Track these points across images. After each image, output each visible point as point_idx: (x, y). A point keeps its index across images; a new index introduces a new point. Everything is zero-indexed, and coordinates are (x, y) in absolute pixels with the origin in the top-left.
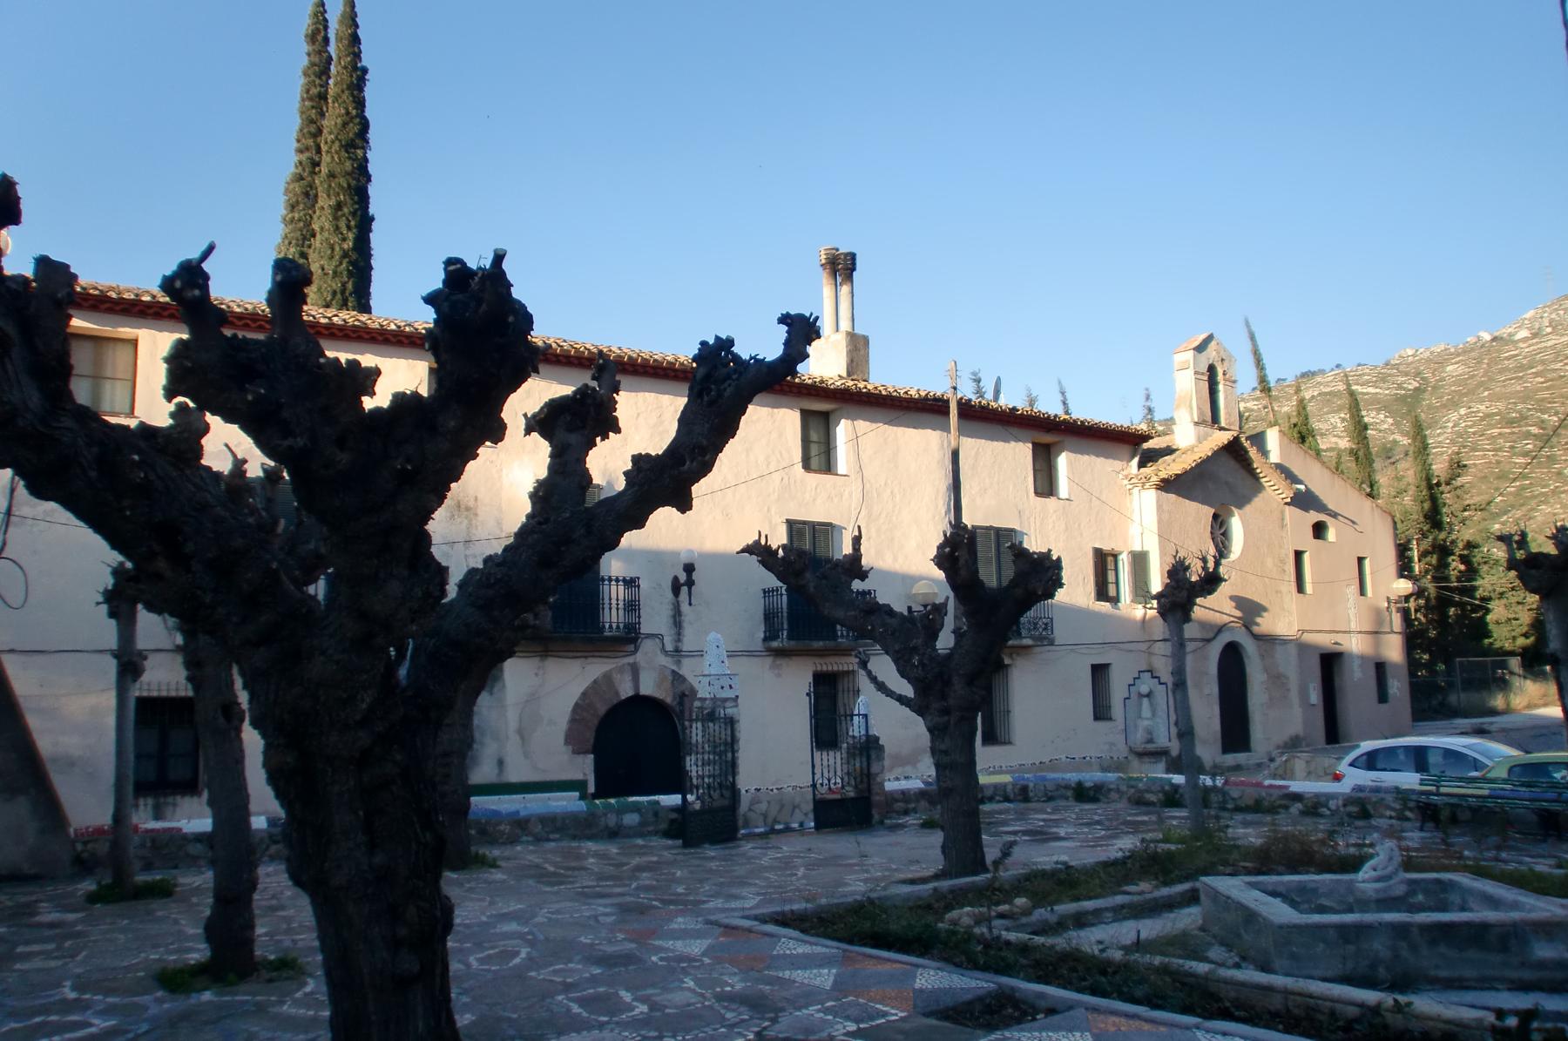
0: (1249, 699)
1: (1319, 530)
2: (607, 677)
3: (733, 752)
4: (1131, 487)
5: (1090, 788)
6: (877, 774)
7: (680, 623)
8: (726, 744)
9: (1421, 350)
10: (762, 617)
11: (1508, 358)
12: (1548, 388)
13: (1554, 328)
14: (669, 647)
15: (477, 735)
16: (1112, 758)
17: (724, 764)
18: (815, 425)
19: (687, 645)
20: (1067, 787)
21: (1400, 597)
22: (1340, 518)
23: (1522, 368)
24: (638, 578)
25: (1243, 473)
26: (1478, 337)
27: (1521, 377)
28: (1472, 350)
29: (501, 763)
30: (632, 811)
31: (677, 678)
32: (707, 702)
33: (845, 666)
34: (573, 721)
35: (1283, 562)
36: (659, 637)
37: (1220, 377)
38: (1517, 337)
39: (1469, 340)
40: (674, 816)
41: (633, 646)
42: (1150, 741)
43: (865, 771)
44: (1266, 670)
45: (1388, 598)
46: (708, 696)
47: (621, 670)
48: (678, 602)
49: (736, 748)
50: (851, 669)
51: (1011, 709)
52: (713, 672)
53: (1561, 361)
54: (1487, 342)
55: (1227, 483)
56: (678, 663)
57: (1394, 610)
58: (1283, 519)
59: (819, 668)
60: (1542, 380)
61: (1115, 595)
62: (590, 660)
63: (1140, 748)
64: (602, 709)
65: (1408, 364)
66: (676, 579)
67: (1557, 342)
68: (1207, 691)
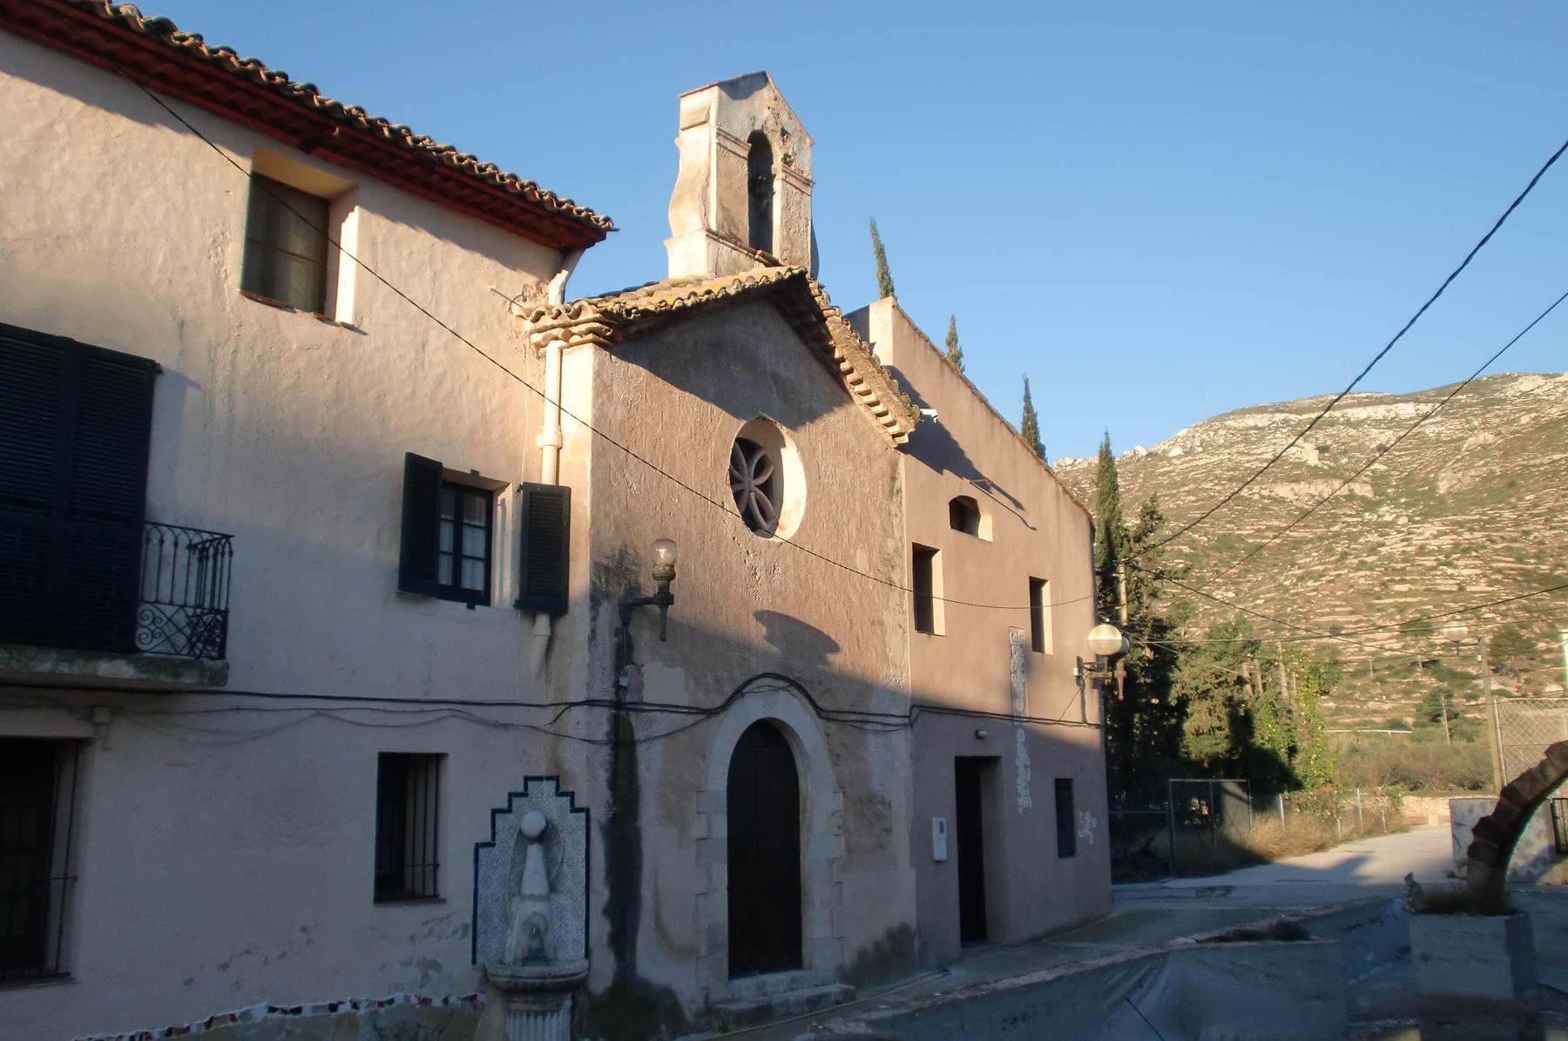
1: (963, 515)
4: (537, 338)
9: (1079, 460)
11: (1162, 474)
12: (1198, 508)
13: (1204, 448)
16: (425, 1001)
21: (1098, 657)
22: (993, 490)
23: (1175, 485)
26: (1135, 451)
27: (1175, 495)
28: (1128, 463)
37: (777, 165)
38: (1172, 454)
39: (1125, 453)
44: (842, 787)
45: (1079, 659)
51: (440, 860)
53: (1211, 481)
54: (1142, 457)
55: (776, 378)
57: (1088, 682)
58: (893, 479)
60: (1194, 499)
61: (479, 586)
63: (503, 976)
65: (1067, 473)
67: (1208, 461)
68: (697, 830)
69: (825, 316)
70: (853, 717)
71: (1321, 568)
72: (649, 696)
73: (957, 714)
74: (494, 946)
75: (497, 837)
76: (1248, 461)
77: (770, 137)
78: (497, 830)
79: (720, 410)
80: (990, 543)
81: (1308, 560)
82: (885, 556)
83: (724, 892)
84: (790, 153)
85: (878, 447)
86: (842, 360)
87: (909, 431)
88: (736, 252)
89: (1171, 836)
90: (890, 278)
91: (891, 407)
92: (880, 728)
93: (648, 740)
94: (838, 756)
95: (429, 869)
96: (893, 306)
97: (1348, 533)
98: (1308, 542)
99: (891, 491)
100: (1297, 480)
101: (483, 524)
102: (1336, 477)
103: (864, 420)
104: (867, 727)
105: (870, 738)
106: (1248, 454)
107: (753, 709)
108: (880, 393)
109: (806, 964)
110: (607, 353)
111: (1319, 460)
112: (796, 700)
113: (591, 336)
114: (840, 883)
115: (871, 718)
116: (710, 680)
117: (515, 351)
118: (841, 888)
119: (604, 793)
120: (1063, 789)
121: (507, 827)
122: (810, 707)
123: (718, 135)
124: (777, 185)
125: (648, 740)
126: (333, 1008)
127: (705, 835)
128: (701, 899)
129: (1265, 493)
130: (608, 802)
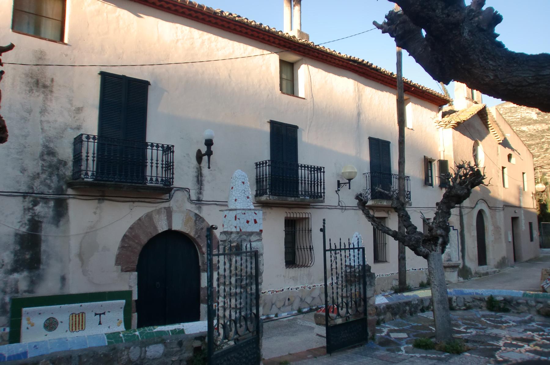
0: (486, 238)
2: (149, 216)
3: (257, 284)
5: (500, 302)
6: (369, 298)
7: (201, 181)
8: (251, 276)
10: (255, 181)
14: (194, 197)
15: (43, 257)
17: (249, 296)
18: (287, 69)
19: (206, 197)
20: (481, 300)
24: (173, 146)
25: (484, 126)
29: (63, 279)
30: (157, 343)
31: (199, 218)
32: (233, 236)
33: (307, 215)
34: (122, 247)
35: (498, 172)
36: (187, 190)
40: (197, 344)
41: (168, 195)
42: (449, 260)
43: (362, 296)
45: (532, 192)
46: (234, 230)
47: (159, 212)
48: (200, 167)
49: (260, 281)
50: (307, 216)
52: (238, 207)
55: (478, 130)
56: (199, 208)
58: (498, 151)
59: (289, 216)
62: (136, 204)
64: (144, 240)
66: (199, 151)
68: (473, 235)
70: (494, 208)
71: (538, 154)
76: (512, 119)
81: (533, 151)
89: (542, 238)
91: (499, 134)
93: (465, 214)
95: (384, 244)
97: (548, 142)
98: (533, 145)
100: (529, 124)
102: (543, 123)
104: (497, 210)
105: (497, 213)
106: (512, 117)
107: (479, 207)
109: (488, 263)
111: (537, 117)
113: (452, 127)
114: (494, 246)
115: (497, 208)
119: (459, 226)
120: (530, 224)
125: (465, 214)
126: (420, 269)
129: (518, 129)
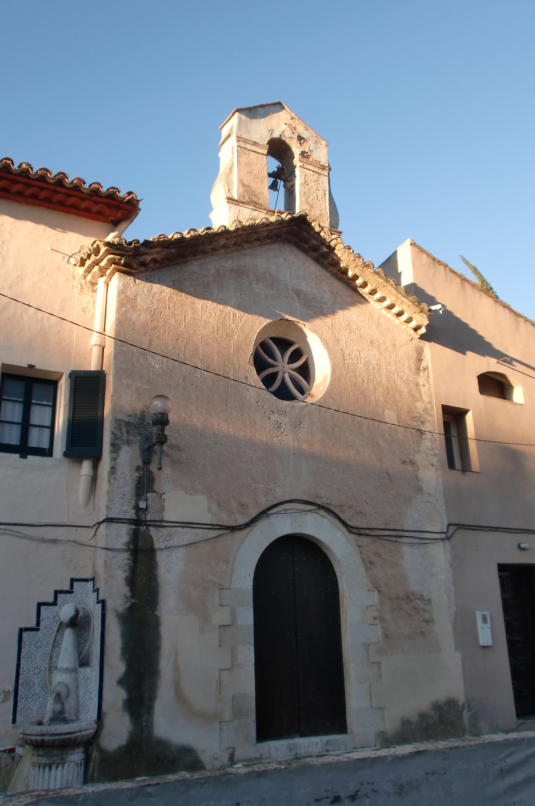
22: (515, 363)
55: (298, 293)
69: (333, 246)
70: (387, 533)
72: (169, 515)
73: (497, 531)
74: (35, 708)
75: (42, 624)
77: (288, 141)
78: (41, 618)
79: (242, 313)
80: (521, 405)
82: (414, 414)
83: (252, 669)
84: (307, 151)
85: (403, 338)
86: (356, 277)
87: (425, 324)
88: (256, 212)
90: (487, 283)
92: (416, 541)
94: (371, 563)
96: (411, 244)
99: (418, 369)
101: (51, 404)
103: (388, 320)
105: (405, 549)
108: (393, 298)
109: (349, 730)
110: (132, 278)
112: (325, 520)
116: (234, 504)
117: (71, 287)
118: (380, 668)
121: (52, 616)
122: (340, 525)
123: (238, 141)
124: (297, 171)
125: (161, 549)
127: (229, 622)
128: (225, 674)
130: (125, 596)
